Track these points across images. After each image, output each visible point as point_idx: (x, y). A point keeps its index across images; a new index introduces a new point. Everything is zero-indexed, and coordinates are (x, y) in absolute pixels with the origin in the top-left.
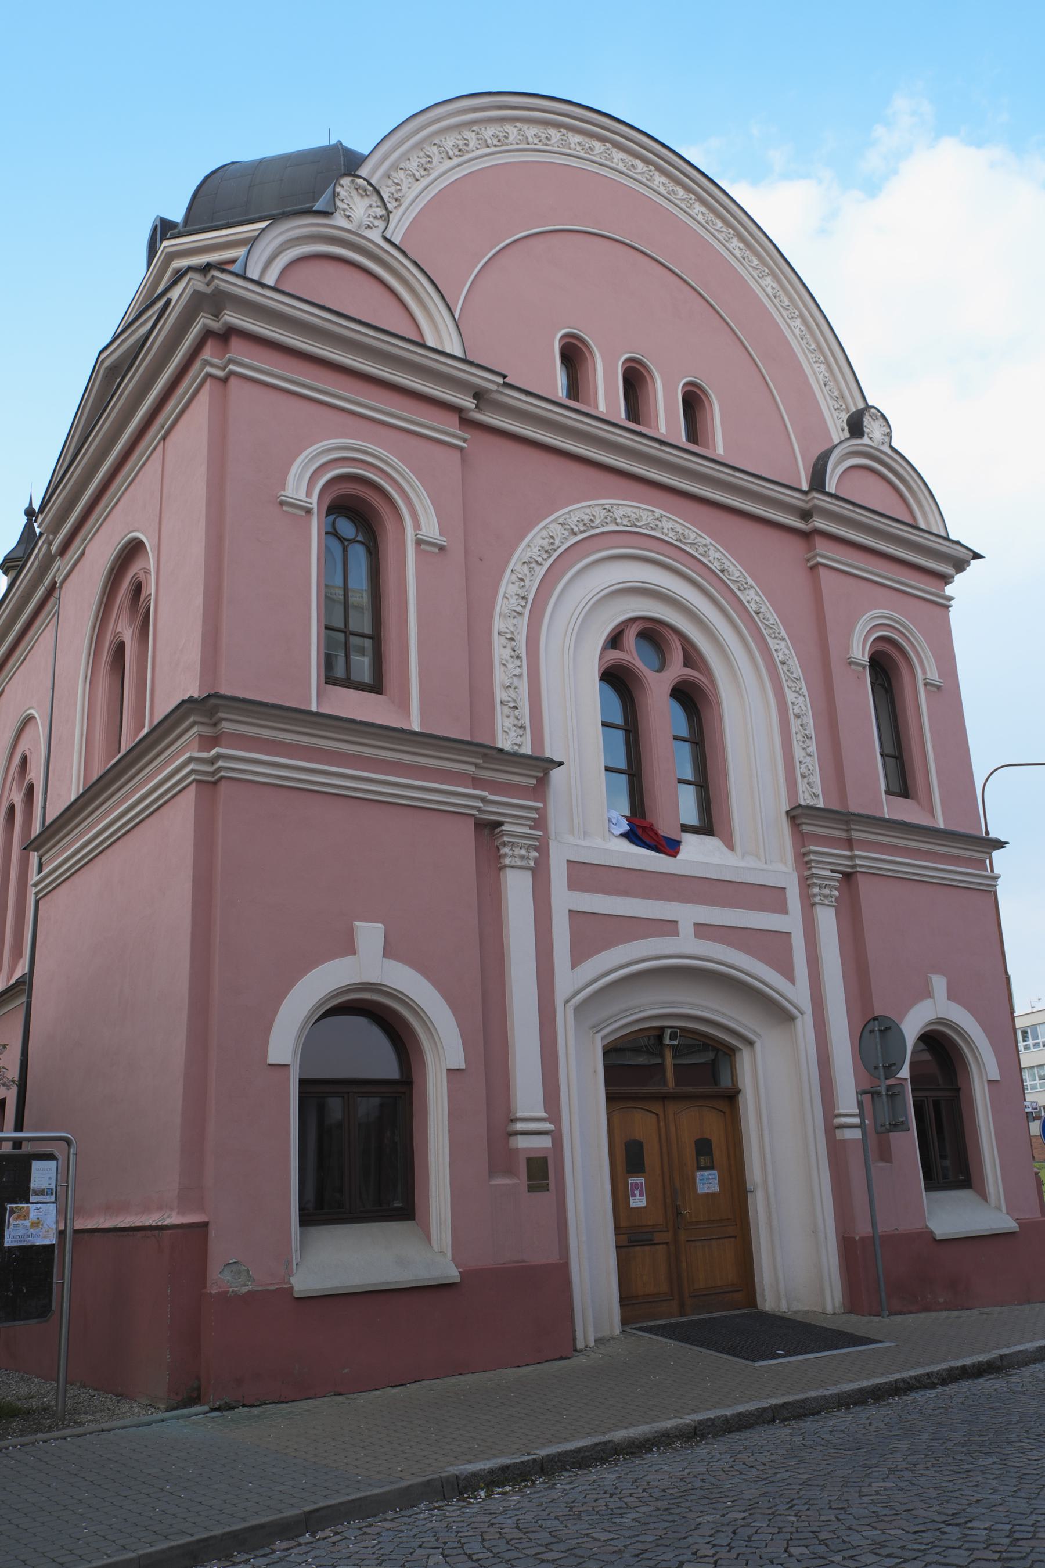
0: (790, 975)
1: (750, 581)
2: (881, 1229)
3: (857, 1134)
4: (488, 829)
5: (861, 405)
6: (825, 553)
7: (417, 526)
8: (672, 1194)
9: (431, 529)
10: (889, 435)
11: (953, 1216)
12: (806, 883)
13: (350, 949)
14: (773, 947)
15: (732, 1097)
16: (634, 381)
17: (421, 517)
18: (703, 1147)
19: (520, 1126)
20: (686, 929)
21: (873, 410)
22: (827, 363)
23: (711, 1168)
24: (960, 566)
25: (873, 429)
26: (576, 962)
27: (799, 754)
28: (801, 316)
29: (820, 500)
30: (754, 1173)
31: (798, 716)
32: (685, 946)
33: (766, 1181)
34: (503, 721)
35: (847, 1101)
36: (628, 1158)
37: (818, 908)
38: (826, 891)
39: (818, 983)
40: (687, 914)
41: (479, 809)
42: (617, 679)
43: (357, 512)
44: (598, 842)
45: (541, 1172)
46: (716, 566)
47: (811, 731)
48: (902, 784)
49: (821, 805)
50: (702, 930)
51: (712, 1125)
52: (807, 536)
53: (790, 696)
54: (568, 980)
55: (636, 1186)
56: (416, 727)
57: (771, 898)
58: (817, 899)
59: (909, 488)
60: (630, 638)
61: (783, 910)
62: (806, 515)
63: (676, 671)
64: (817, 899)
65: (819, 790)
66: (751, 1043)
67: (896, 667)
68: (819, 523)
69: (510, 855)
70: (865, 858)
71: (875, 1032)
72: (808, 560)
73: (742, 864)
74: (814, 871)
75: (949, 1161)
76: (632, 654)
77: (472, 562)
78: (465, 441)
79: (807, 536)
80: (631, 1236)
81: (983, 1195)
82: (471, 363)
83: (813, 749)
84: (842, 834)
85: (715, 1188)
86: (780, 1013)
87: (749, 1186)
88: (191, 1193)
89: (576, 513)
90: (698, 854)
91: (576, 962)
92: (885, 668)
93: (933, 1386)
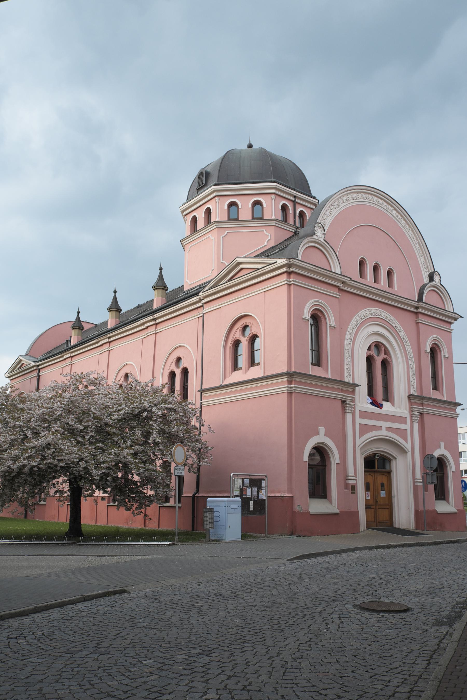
0: (406, 441)
1: (402, 329)
2: (426, 509)
3: (421, 484)
4: (344, 402)
5: (433, 271)
6: (422, 319)
7: (330, 322)
8: (375, 496)
9: (333, 323)
10: (440, 280)
11: (442, 507)
12: (411, 416)
13: (318, 434)
14: (402, 433)
15: (389, 473)
16: (376, 268)
17: (331, 320)
18: (382, 485)
19: (350, 478)
20: (384, 428)
21: (436, 273)
22: (424, 257)
23: (384, 490)
24: (456, 319)
25: (436, 278)
26: (361, 436)
27: (411, 379)
28: (419, 243)
29: (421, 304)
30: (394, 492)
31: (412, 368)
32: (383, 433)
33: (398, 495)
34: (346, 374)
35: (419, 475)
36: (367, 487)
37: (414, 423)
38: (416, 418)
39: (412, 444)
40: (384, 424)
41: (343, 398)
42: (370, 360)
43: (317, 318)
44: (364, 405)
45: (354, 489)
46: (394, 325)
47: (415, 373)
48: (435, 387)
49: (416, 394)
50: (388, 429)
51: (384, 479)
52: (416, 313)
53: (410, 362)
54: (359, 441)
55: (368, 494)
56: (330, 377)
57: (402, 420)
58: (414, 421)
59: (444, 295)
60: (373, 347)
61: (406, 423)
62: (417, 308)
63: (383, 356)
64: (414, 421)
65: (416, 390)
66: (395, 458)
67: (437, 351)
68: (421, 310)
69: (348, 409)
70: (427, 409)
71: (427, 457)
72: (416, 321)
73: (396, 411)
74: (414, 413)
75: (441, 494)
76: (373, 352)
77: (340, 330)
78: (339, 296)
79: (416, 313)
80: (368, 507)
81: (448, 502)
82: (344, 276)
83: (415, 378)
84: (420, 402)
85: (385, 496)
86: (403, 451)
87: (393, 496)
88: (290, 489)
89: (363, 313)
90: (387, 406)
91: (361, 436)
92: (434, 351)
93: (445, 544)
